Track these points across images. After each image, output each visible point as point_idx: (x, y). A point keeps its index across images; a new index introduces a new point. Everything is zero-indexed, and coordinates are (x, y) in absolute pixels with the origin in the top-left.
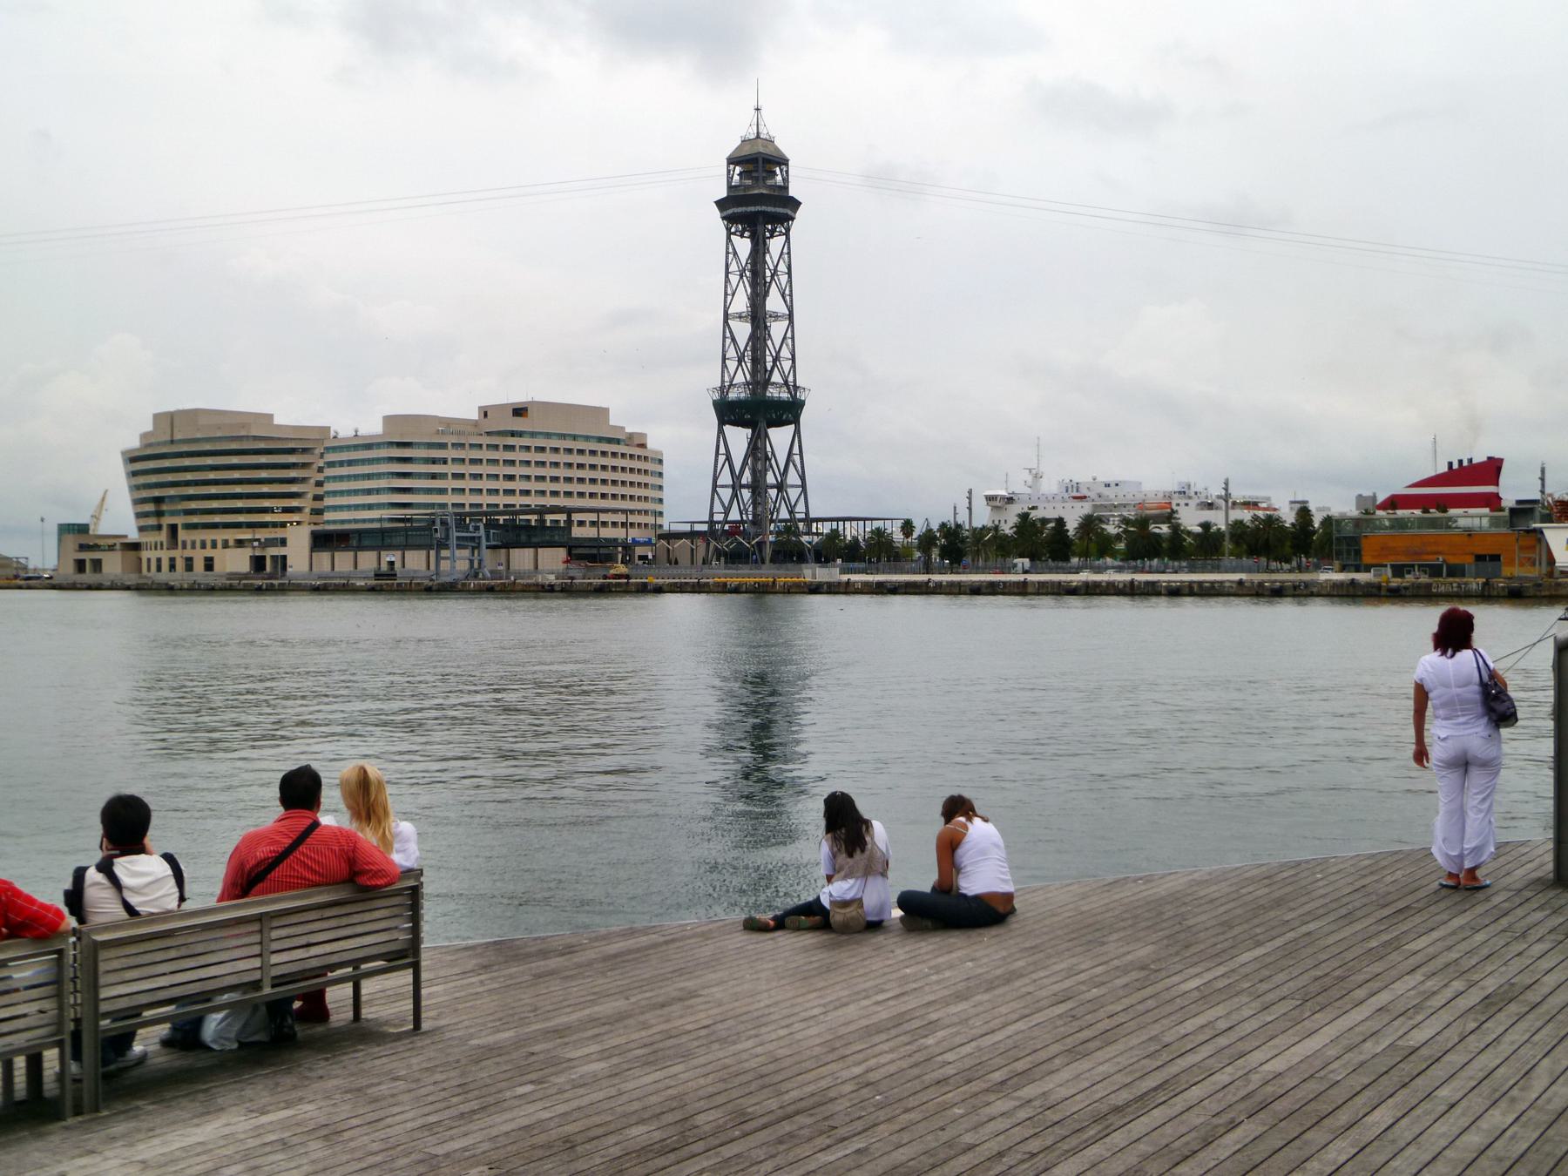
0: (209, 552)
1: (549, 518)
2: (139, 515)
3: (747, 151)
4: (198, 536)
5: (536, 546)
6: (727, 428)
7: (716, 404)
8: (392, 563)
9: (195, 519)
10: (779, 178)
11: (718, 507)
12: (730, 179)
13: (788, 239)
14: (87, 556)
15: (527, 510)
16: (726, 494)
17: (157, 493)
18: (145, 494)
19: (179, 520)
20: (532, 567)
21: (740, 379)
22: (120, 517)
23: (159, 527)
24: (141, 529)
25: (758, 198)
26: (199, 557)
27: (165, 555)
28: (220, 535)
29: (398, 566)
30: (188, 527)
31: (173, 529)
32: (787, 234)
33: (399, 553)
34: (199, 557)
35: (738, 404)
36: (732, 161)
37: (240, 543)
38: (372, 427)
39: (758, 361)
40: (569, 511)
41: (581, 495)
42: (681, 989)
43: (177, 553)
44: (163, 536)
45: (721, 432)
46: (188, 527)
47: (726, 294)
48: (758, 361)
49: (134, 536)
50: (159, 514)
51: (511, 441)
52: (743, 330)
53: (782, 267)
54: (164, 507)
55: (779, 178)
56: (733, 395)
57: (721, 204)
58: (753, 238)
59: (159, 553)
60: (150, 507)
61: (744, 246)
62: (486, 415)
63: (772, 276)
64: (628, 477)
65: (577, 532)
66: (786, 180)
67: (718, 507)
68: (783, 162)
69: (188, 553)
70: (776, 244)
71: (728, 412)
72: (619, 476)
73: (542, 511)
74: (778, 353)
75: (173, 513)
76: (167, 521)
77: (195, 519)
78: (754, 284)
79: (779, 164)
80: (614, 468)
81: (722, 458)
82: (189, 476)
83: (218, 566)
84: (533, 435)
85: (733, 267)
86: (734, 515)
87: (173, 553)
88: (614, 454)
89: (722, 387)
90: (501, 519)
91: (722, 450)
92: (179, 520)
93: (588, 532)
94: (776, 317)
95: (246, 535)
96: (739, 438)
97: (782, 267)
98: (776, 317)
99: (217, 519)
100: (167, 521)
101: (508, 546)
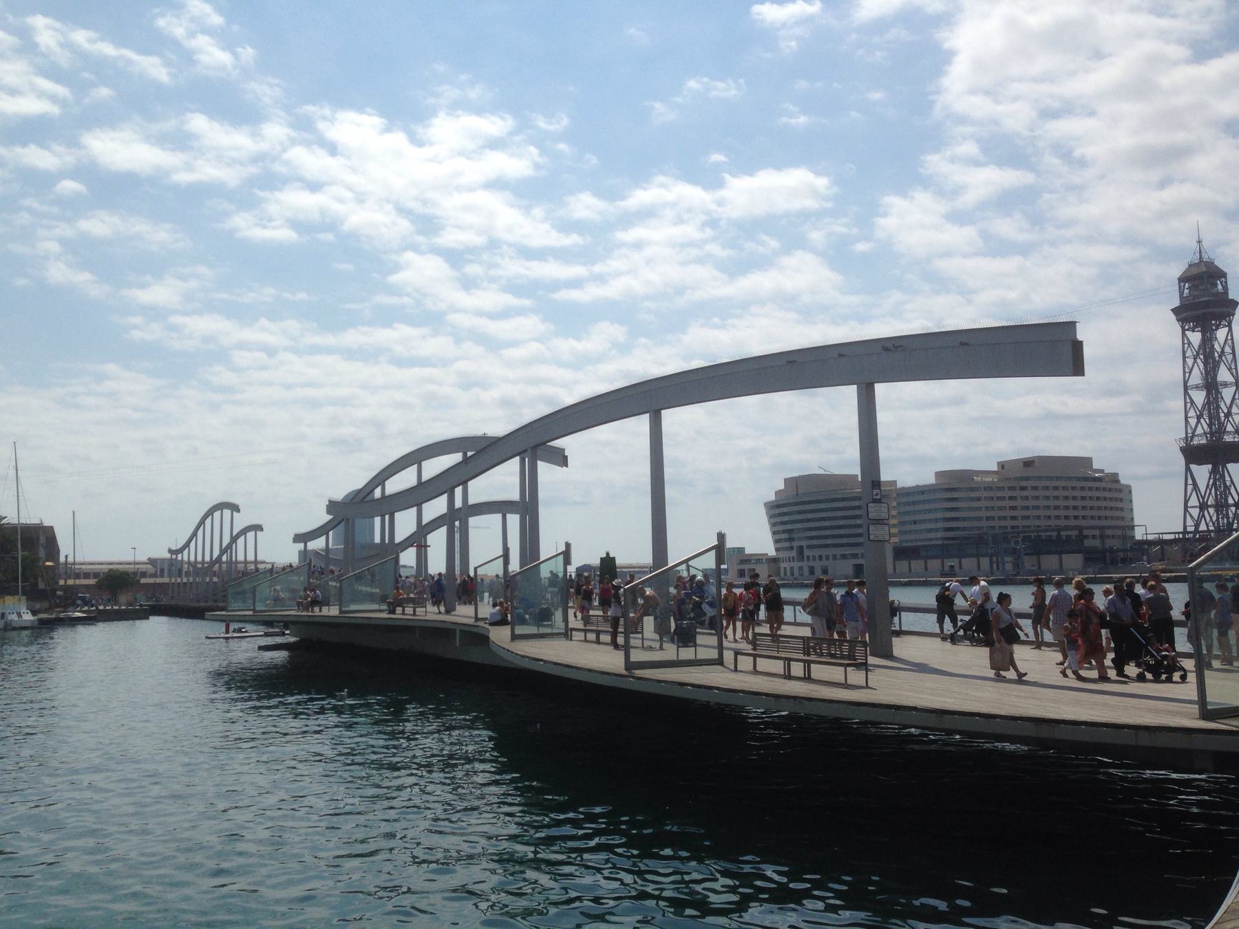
0: (824, 563)
1: (1063, 533)
2: (776, 541)
3: (1194, 271)
4: (817, 552)
5: (1060, 553)
6: (1193, 467)
7: (1183, 450)
8: (952, 567)
9: (815, 542)
10: (1220, 287)
11: (1190, 522)
12: (1181, 293)
13: (1230, 330)
14: (746, 567)
15: (1067, 528)
16: (1195, 512)
17: (789, 527)
18: (1118, 514)
19: (804, 543)
20: (1058, 567)
21: (1199, 431)
22: (758, 539)
23: (792, 548)
24: (777, 550)
25: (926, 569)
26: (818, 565)
27: (796, 565)
28: (830, 552)
29: (957, 568)
30: (809, 547)
31: (801, 549)
32: (1230, 326)
33: (956, 561)
34: (818, 565)
35: (1200, 447)
36: (1182, 280)
37: (844, 557)
38: (929, 479)
39: (1214, 417)
40: (1080, 529)
41: (1092, 517)
42: (182, 141)
43: (805, 564)
44: (794, 553)
45: (1188, 469)
46: (809, 547)
47: (1184, 372)
48: (1214, 417)
49: (772, 552)
50: (791, 540)
51: (1024, 484)
52: (1199, 397)
53: (1190, 362)
54: (794, 536)
55: (1220, 287)
56: (1195, 442)
57: (1175, 311)
58: (1204, 333)
59: (792, 564)
60: (785, 536)
61: (1196, 337)
62: (1003, 467)
63: (1220, 356)
64: (1095, 503)
65: (1088, 543)
66: (1225, 288)
67: (1190, 522)
68: (1223, 275)
69: (811, 563)
70: (1221, 334)
71: (1193, 454)
72: (1088, 503)
73: (1059, 529)
74: (1198, 421)
75: (800, 539)
76: (796, 544)
77: (815, 542)
78: (1205, 363)
79: (1219, 278)
80: (1098, 498)
81: (1190, 488)
82: (824, 515)
83: (830, 572)
84: (1040, 478)
85: (1189, 353)
86: (1203, 527)
87: (801, 564)
88: (1097, 489)
89: (1186, 437)
90: (1033, 535)
91: (1190, 481)
92: (804, 543)
93: (1096, 543)
94: (1197, 387)
95: (847, 551)
96: (1202, 473)
97: (1190, 362)
98: (1197, 387)
99: (844, 541)
100: (796, 544)
101: (1038, 553)
